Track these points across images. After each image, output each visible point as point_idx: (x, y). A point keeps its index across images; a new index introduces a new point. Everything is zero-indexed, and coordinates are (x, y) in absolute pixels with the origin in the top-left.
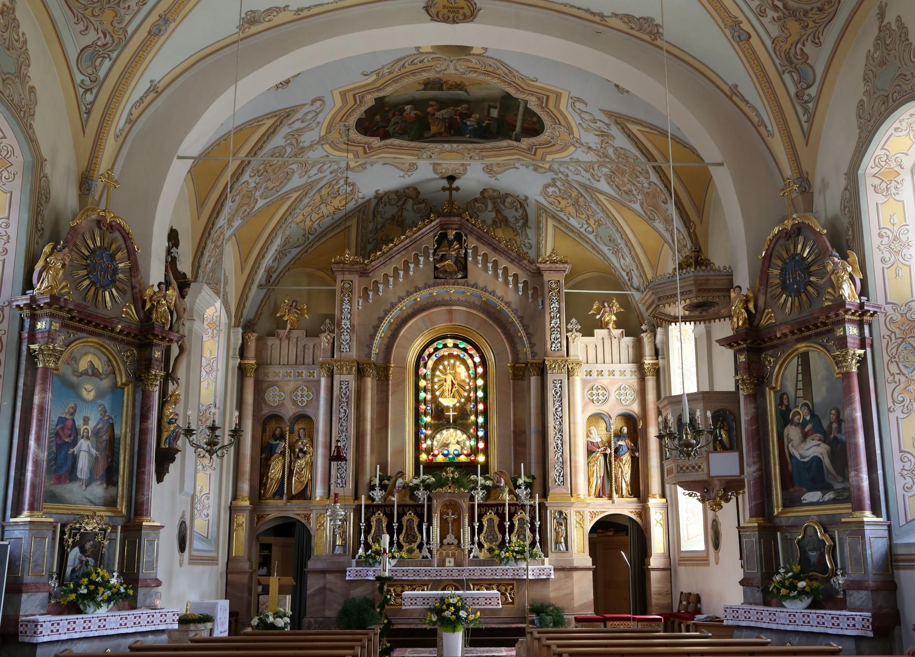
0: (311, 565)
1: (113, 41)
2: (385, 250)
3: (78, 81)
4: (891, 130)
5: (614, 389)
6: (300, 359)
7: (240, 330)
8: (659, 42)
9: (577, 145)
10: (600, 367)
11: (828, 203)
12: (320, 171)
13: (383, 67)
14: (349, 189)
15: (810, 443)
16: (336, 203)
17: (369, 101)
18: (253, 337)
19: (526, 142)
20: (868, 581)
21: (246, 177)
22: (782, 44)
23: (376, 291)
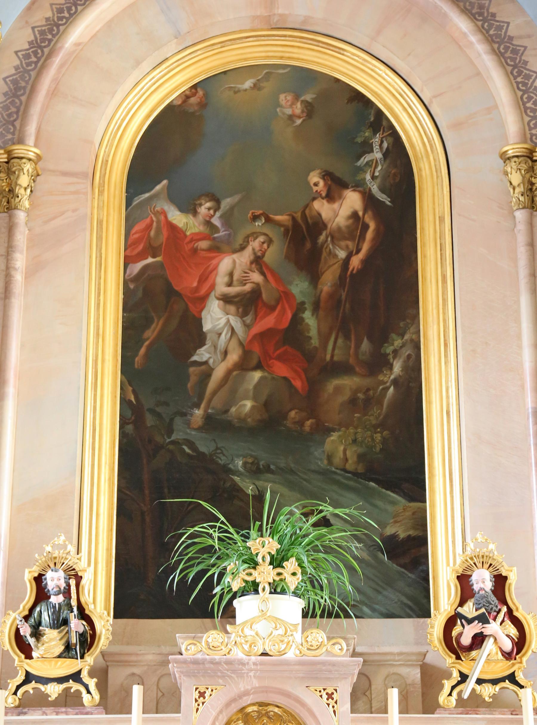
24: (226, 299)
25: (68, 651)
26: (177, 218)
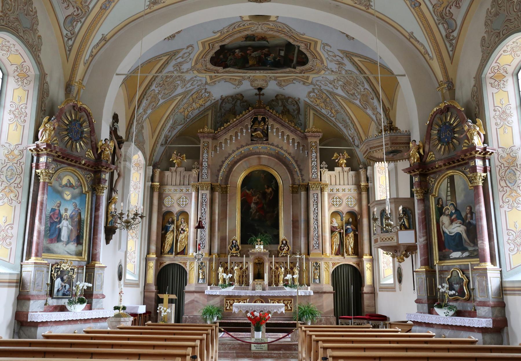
0: (187, 288)
1: (82, 12)
2: (226, 126)
3: (64, 34)
4: (501, 52)
6: (182, 182)
7: (151, 167)
8: (370, 10)
9: (326, 70)
10: (338, 187)
11: (464, 92)
12: (192, 85)
13: (224, 28)
14: (207, 95)
15: (455, 225)
16: (201, 102)
17: (217, 48)
18: (158, 171)
19: (299, 69)
20: (489, 301)
21: (153, 87)
22: (438, 8)
23: (221, 147)
24: (254, 203)
25: (236, 250)
26: (247, 191)
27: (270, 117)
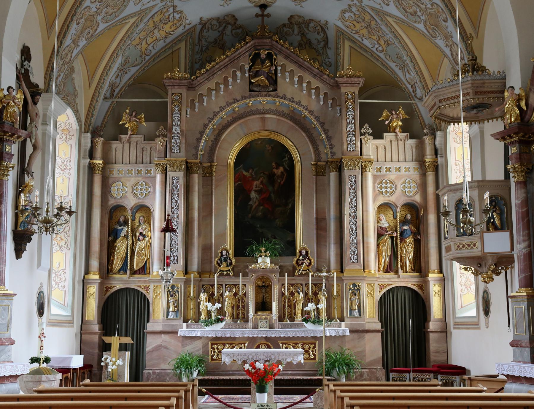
0: (150, 327)
5: (401, 182)
6: (139, 159)
7: (89, 135)
10: (388, 165)
14: (177, 16)
16: (167, 28)
18: (100, 141)
23: (201, 102)
24: (255, 191)
25: (227, 266)
26: (245, 173)
27: (280, 52)
